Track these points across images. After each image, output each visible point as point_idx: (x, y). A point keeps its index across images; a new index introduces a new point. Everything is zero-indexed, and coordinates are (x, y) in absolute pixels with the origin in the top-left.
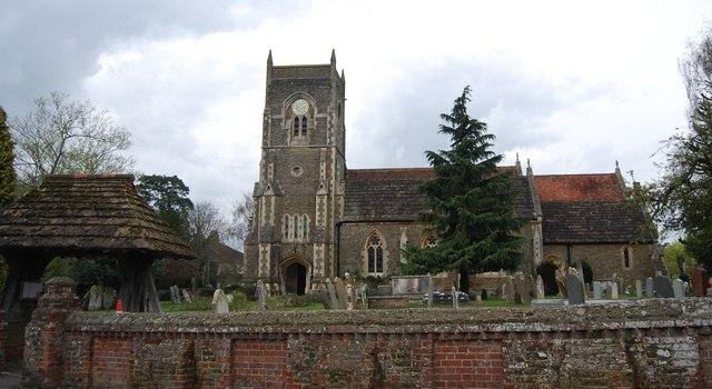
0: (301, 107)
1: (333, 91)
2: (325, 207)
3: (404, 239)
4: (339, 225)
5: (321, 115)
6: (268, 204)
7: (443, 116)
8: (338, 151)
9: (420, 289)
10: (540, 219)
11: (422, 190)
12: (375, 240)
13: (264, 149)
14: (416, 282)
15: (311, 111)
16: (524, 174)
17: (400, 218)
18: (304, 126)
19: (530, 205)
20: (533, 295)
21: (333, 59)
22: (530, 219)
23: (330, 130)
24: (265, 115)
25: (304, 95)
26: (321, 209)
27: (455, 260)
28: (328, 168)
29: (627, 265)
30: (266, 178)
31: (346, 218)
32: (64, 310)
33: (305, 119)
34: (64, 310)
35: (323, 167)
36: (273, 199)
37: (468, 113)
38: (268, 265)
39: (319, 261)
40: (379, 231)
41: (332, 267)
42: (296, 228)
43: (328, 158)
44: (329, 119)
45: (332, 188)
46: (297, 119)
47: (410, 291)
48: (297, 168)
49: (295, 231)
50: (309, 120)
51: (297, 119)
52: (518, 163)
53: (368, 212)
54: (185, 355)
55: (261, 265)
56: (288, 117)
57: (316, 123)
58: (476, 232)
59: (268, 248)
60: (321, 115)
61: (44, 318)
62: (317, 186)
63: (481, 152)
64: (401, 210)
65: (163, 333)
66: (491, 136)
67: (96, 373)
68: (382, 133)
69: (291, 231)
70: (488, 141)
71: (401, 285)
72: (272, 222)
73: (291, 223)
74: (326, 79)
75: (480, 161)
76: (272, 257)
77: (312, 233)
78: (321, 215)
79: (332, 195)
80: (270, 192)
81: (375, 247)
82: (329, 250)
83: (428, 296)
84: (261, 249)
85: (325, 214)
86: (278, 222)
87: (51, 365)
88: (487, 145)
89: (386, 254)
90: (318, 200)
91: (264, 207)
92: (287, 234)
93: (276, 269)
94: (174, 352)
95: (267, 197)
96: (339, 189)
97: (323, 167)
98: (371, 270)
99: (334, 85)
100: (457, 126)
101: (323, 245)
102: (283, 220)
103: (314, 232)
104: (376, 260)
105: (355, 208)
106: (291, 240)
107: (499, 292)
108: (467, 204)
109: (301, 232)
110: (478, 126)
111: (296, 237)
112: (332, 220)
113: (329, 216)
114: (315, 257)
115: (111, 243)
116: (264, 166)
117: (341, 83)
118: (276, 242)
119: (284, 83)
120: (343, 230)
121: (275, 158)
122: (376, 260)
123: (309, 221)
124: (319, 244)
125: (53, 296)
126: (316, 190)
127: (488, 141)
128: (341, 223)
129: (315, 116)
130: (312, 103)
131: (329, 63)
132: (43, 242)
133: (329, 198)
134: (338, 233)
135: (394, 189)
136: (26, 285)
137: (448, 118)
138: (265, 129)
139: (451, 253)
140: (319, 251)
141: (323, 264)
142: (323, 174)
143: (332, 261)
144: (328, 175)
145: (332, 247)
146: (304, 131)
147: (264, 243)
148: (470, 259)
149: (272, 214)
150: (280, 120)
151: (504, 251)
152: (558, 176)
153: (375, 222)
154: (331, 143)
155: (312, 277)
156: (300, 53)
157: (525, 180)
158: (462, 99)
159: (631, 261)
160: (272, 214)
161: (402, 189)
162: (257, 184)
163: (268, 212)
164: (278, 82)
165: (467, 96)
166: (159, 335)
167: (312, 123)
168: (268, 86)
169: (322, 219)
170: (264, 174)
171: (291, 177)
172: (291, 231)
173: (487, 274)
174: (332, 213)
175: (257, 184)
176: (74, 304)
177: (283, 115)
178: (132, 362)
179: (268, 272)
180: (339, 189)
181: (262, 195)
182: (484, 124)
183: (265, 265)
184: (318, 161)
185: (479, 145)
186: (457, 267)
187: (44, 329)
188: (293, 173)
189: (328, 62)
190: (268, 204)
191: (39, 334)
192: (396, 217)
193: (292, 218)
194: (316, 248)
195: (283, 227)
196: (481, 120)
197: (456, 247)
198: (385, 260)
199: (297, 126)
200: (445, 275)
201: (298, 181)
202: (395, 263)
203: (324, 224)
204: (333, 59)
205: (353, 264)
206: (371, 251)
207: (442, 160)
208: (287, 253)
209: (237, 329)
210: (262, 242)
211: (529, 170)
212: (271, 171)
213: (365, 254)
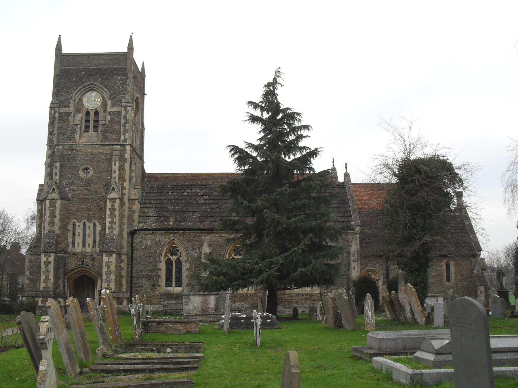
0: (92, 100)
1: (130, 82)
2: (117, 213)
3: (206, 249)
4: (132, 233)
5: (114, 109)
6: (53, 209)
7: (251, 103)
8: (133, 150)
9: (217, 309)
10: (357, 229)
12: (173, 251)
14: (212, 300)
15: (104, 104)
16: (341, 178)
18: (96, 121)
19: (346, 214)
21: (131, 47)
22: (347, 229)
23: (124, 125)
24: (51, 108)
25: (97, 89)
26: (112, 215)
27: (260, 272)
29: (448, 280)
31: (141, 226)
33: (97, 113)
35: (116, 167)
36: (58, 203)
37: (280, 99)
38: (51, 277)
39: (108, 273)
40: (178, 240)
41: (124, 281)
43: (122, 158)
44: (123, 113)
45: (126, 192)
46: (88, 113)
47: (205, 311)
49: (82, 241)
50: (101, 114)
52: (334, 169)
53: (167, 219)
55: (43, 277)
56: (78, 111)
57: (109, 118)
58: (286, 237)
59: (52, 258)
60: (114, 109)
62: (108, 188)
63: (292, 147)
64: (203, 218)
66: (306, 127)
68: (191, 134)
69: (79, 239)
70: (303, 132)
71: (195, 302)
72: (56, 229)
73: (79, 230)
74: (121, 69)
75: (292, 157)
76: (57, 268)
77: (102, 242)
78: (112, 222)
79: (126, 199)
80: (55, 195)
81: (173, 258)
82: (122, 261)
83: (225, 319)
84: (43, 259)
85: (116, 220)
86: (64, 228)
88: (301, 137)
89: (185, 266)
90: (109, 205)
91: (48, 212)
92: (74, 243)
93: (61, 281)
95: (52, 200)
96: (134, 193)
97: (116, 167)
98: (169, 284)
99: (130, 75)
100: (266, 116)
101: (114, 256)
102: (70, 227)
103: (105, 244)
104: (174, 275)
105: (152, 215)
107: (313, 311)
111: (84, 245)
112: (125, 227)
113: (122, 223)
114: (105, 269)
116: (50, 166)
117: (140, 77)
118: (60, 252)
119: (75, 73)
120: (138, 239)
121: (62, 157)
122: (174, 275)
123: (99, 228)
124: (109, 253)
126: (107, 193)
127: (303, 132)
129: (109, 109)
130: (105, 95)
131: (125, 50)
133: (122, 203)
134: (132, 243)
137: (256, 106)
139: (257, 263)
140: (109, 263)
141: (113, 277)
142: (116, 175)
143: (124, 273)
144: (121, 177)
145: (124, 257)
146: (96, 127)
147: (47, 253)
148: (278, 270)
149: (57, 220)
150: (68, 114)
151: (319, 263)
154: (125, 140)
157: (342, 186)
159: (453, 276)
160: (57, 220)
161: (205, 194)
165: (278, 80)
167: (105, 118)
168: (56, 76)
169: (114, 226)
170: (49, 175)
171: (79, 178)
172: (79, 239)
173: (298, 291)
174: (125, 220)
177: (72, 109)
179: (51, 286)
180: (133, 192)
181: (45, 199)
182: (299, 114)
183: (47, 279)
184: (110, 161)
185: (292, 137)
186: (262, 282)
188: (82, 174)
189: (124, 49)
190: (53, 209)
192: (199, 225)
193: (79, 226)
194: (105, 258)
195: (70, 235)
196: (295, 109)
197: (263, 257)
198: (185, 273)
199: (87, 121)
200: (250, 290)
201: (88, 183)
202: (195, 277)
203: (116, 232)
204: (131, 47)
205: (149, 277)
206: (169, 263)
207: (249, 156)
208: (73, 264)
210: (45, 251)
211: (347, 175)
212: (57, 171)
213: (162, 266)
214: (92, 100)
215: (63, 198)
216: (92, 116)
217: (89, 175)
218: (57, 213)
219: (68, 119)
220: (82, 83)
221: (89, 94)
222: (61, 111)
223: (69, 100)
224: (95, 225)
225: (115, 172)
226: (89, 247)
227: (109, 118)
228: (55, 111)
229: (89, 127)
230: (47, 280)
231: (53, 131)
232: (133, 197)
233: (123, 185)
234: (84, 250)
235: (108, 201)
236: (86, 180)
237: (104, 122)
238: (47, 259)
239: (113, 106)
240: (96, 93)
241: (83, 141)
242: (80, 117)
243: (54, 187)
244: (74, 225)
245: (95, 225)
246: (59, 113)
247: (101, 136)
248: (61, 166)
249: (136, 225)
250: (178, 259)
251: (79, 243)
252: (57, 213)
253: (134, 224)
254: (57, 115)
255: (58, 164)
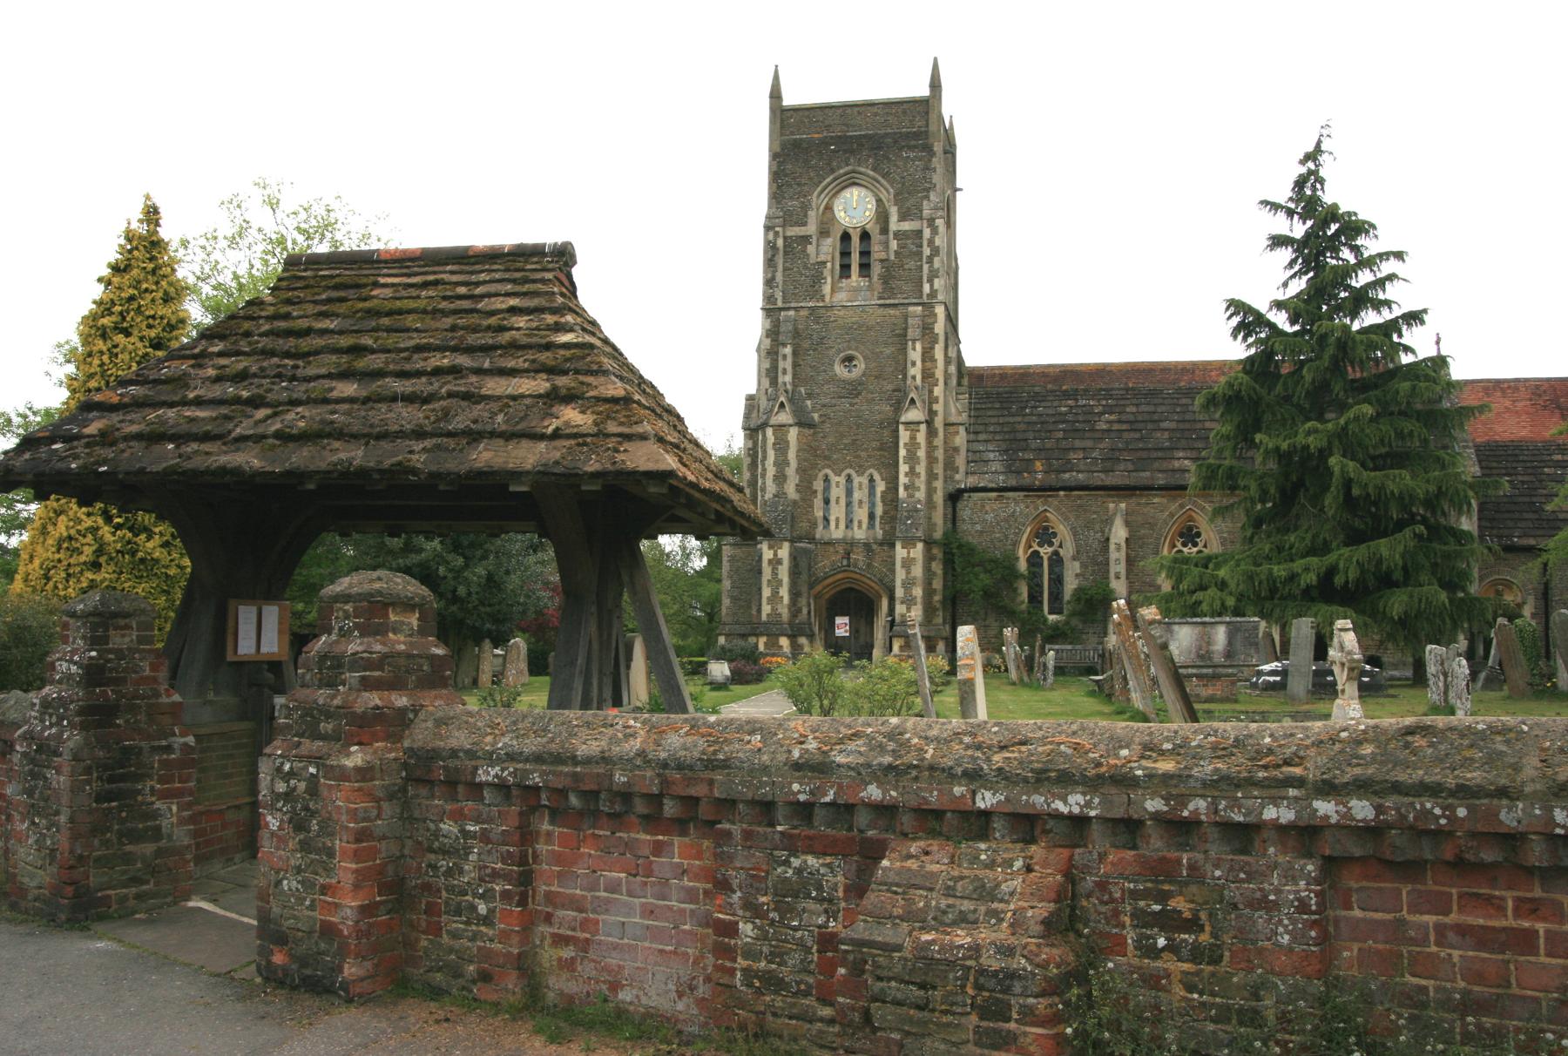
0: (854, 207)
2: (921, 453)
4: (954, 497)
5: (907, 226)
6: (781, 446)
9: (1229, 654)
11: (1212, 401)
12: (1045, 535)
13: (770, 310)
15: (882, 217)
17: (1110, 480)
18: (865, 254)
20: (1324, 687)
21: (935, 85)
23: (930, 260)
24: (768, 228)
26: (912, 458)
28: (928, 355)
30: (774, 382)
31: (972, 481)
32: (401, 701)
33: (865, 236)
34: (401, 701)
35: (915, 354)
36: (793, 434)
38: (784, 592)
39: (908, 584)
42: (849, 504)
44: (927, 233)
46: (846, 237)
48: (850, 359)
51: (846, 237)
54: (1050, 927)
55: (766, 592)
56: (824, 233)
57: (894, 245)
59: (784, 552)
60: (907, 226)
61: (326, 727)
64: (1111, 461)
65: (884, 811)
67: (549, 955)
69: (838, 512)
70: (1387, 268)
73: (837, 492)
74: (916, 135)
76: (795, 573)
78: (912, 473)
79: (939, 422)
80: (785, 417)
81: (1045, 551)
84: (767, 554)
85: (921, 469)
86: (805, 488)
87: (366, 910)
90: (904, 436)
92: (826, 520)
93: (803, 601)
94: (994, 911)
95: (780, 428)
97: (915, 354)
99: (938, 147)
101: (920, 546)
102: (818, 485)
106: (837, 533)
108: (1346, 442)
109: (862, 514)
110: (1354, 228)
112: (939, 484)
113: (931, 476)
115: (528, 456)
118: (800, 539)
119: (814, 146)
120: (966, 510)
123: (881, 487)
124: (909, 542)
125: (354, 647)
128: (960, 492)
129: (894, 225)
130: (884, 196)
132: (300, 457)
133: (932, 432)
134: (953, 518)
135: (1089, 411)
136: (246, 615)
138: (770, 262)
141: (918, 592)
142: (916, 371)
144: (928, 375)
146: (865, 268)
149: (791, 471)
150: (805, 240)
152: (1498, 382)
153: (1046, 490)
155: (892, 623)
156: (853, 71)
158: (1313, 156)
160: (791, 471)
162: (750, 398)
163: (781, 464)
164: (796, 144)
166: (862, 818)
167: (886, 245)
168: (774, 156)
169: (916, 482)
170: (770, 373)
171: (834, 379)
172: (838, 512)
174: (939, 469)
175: (750, 398)
176: (436, 677)
177: (811, 228)
178: (730, 929)
179: (784, 612)
180: (952, 406)
181: (764, 425)
184: (902, 340)
185: (1364, 278)
187: (330, 772)
188: (840, 370)
189: (923, 91)
190: (781, 446)
191: (313, 789)
192: (1100, 478)
195: (818, 502)
199: (845, 254)
201: (853, 389)
203: (921, 495)
204: (935, 85)
208: (824, 564)
209: (1362, 809)
214: (854, 207)
215: (803, 423)
216: (855, 240)
217: (856, 373)
218: (792, 455)
219: (804, 251)
220: (833, 171)
221: (847, 194)
222: (789, 234)
223: (805, 208)
224: (872, 480)
225: (914, 364)
226: (860, 527)
227: (894, 245)
228: (777, 233)
229: (849, 266)
230: (775, 597)
231: (773, 278)
232: (953, 419)
233: (931, 392)
234: (850, 534)
235: (901, 427)
236: (850, 383)
237: (883, 255)
238: (775, 554)
239: (903, 217)
240: (863, 191)
241: (841, 297)
242: (828, 249)
243: (782, 399)
244: (827, 480)
245: (872, 480)
246: (785, 238)
247: (878, 286)
248: (795, 353)
249: (962, 480)
250: (1056, 553)
251: (837, 520)
252: (792, 455)
253: (957, 477)
254: (780, 242)
255: (788, 350)
